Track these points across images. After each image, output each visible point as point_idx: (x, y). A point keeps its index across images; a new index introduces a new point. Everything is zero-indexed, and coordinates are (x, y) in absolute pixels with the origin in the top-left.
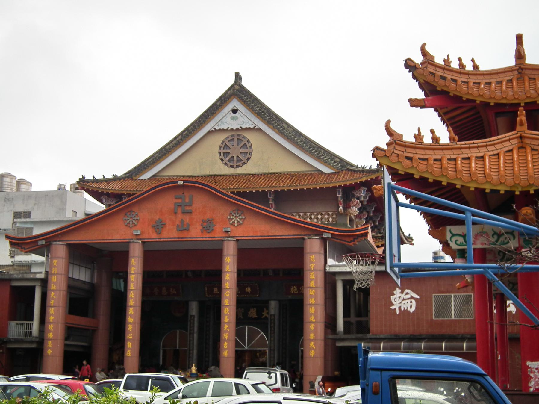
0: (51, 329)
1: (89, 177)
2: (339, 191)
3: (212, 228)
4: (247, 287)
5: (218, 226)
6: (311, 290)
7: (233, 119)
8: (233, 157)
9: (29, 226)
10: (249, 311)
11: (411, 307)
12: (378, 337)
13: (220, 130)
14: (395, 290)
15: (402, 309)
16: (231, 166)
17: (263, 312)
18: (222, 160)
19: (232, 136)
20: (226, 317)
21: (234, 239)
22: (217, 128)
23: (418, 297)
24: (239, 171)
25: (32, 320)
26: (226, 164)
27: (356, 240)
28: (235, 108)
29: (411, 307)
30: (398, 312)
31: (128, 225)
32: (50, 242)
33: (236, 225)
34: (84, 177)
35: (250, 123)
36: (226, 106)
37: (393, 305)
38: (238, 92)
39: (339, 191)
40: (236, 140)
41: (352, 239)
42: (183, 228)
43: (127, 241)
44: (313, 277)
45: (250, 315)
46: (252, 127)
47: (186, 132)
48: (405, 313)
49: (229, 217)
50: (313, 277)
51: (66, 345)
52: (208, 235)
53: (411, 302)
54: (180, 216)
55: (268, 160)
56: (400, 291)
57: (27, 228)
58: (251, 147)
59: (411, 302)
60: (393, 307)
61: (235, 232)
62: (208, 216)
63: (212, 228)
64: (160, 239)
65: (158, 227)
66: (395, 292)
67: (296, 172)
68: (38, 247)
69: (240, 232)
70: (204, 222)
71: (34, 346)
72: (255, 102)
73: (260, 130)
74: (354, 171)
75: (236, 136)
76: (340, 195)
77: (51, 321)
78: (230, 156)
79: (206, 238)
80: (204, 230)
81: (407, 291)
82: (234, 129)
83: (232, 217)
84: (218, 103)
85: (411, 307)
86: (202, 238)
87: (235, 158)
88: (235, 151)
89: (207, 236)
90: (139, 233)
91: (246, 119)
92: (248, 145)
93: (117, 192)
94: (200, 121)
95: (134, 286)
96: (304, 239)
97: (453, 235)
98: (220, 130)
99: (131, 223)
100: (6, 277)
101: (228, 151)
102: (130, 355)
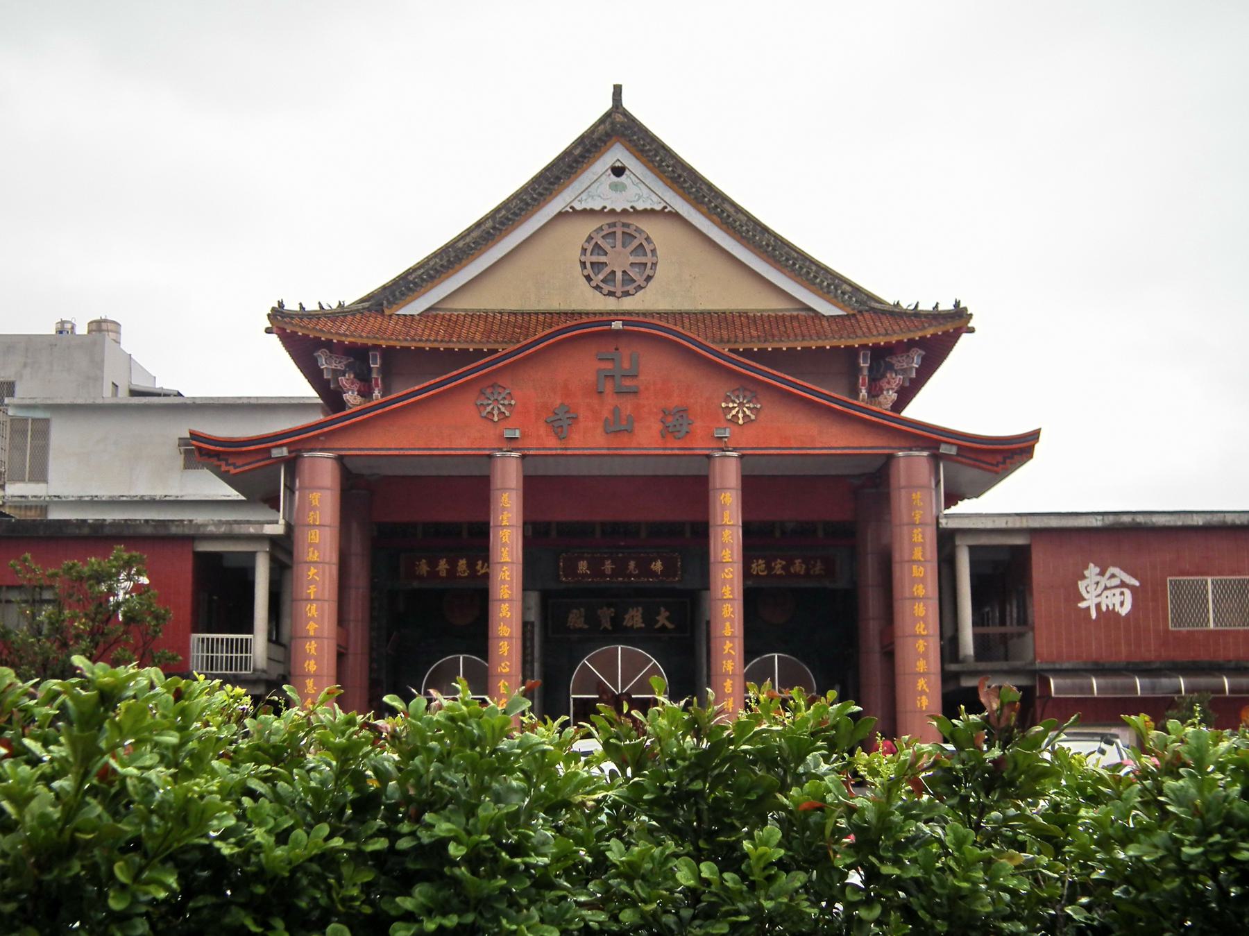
0: (313, 651)
1: (291, 306)
2: (865, 356)
3: (685, 429)
5: (698, 423)
6: (915, 567)
7: (614, 187)
8: (613, 272)
9: (39, 414)
10: (626, 612)
11: (1122, 604)
12: (1058, 666)
13: (585, 211)
14: (1087, 568)
15: (1104, 608)
16: (611, 294)
17: (659, 614)
18: (588, 278)
19: (610, 225)
20: (728, 624)
21: (735, 454)
22: (579, 207)
23: (1137, 583)
24: (628, 304)
25: (250, 630)
26: (597, 288)
28: (618, 164)
30: (1094, 615)
31: (489, 418)
32: (300, 450)
33: (741, 422)
34: (281, 304)
36: (598, 158)
37: (1084, 599)
38: (618, 130)
39: (375, 357)
40: (619, 235)
41: (1000, 458)
42: (619, 428)
43: (487, 452)
44: (918, 538)
45: (627, 622)
46: (658, 208)
47: (503, 212)
48: (1109, 616)
49: (723, 405)
52: (681, 444)
53: (1122, 593)
54: (611, 401)
55: (687, 282)
56: (1097, 570)
57: (34, 420)
58: (653, 251)
59: (1122, 593)
60: (1082, 605)
61: (739, 437)
62: (675, 402)
63: (685, 429)
64: (566, 449)
65: (560, 423)
66: (1086, 573)
67: (759, 311)
68: (267, 462)
69: (750, 439)
70: (665, 413)
72: (662, 152)
73: (675, 215)
74: (884, 312)
76: (864, 364)
78: (607, 270)
79: (672, 449)
80: (667, 432)
81: (1112, 570)
82: (619, 210)
83: (731, 405)
84: (577, 152)
85: (1123, 604)
86: (665, 449)
87: (619, 275)
88: (619, 259)
89: (674, 447)
90: (517, 435)
91: (643, 190)
92: (648, 247)
94: (534, 190)
96: (890, 457)
99: (496, 412)
100: (187, 531)
101: (603, 259)
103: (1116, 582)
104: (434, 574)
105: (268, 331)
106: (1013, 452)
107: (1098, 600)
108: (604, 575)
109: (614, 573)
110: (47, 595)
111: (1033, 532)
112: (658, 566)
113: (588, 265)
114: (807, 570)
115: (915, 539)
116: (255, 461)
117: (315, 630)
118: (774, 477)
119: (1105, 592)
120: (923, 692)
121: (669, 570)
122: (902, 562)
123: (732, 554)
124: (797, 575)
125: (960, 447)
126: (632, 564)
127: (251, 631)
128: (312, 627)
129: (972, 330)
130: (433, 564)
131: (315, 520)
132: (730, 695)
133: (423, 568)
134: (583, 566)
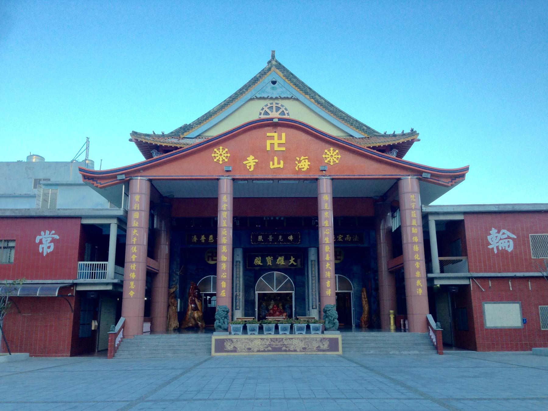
0: (134, 268)
6: (413, 229)
7: (273, 88)
11: (509, 246)
21: (329, 177)
23: (515, 237)
25: (107, 260)
27: (453, 181)
29: (509, 246)
30: (496, 251)
35: (288, 92)
46: (290, 97)
50: (415, 216)
53: (508, 242)
56: (496, 231)
59: (508, 242)
60: (490, 247)
71: (110, 288)
75: (274, 103)
77: (134, 260)
82: (274, 97)
93: (171, 145)
95: (227, 224)
102: (224, 296)
103: (505, 236)
104: (199, 241)
105: (131, 140)
106: (457, 176)
107: (498, 244)
108: (268, 241)
109: (273, 241)
110: (11, 244)
111: (465, 213)
112: (291, 238)
113: (264, 110)
114: (352, 239)
115: (413, 216)
116: (113, 183)
117: (136, 258)
119: (500, 240)
120: (419, 287)
121: (296, 239)
122: (406, 226)
123: (329, 240)
124: (347, 241)
125: (432, 175)
126: (280, 237)
127: (107, 260)
128: (134, 257)
129: (419, 140)
130: (199, 237)
131: (137, 208)
132: (329, 288)
133: (195, 239)
134: (260, 238)
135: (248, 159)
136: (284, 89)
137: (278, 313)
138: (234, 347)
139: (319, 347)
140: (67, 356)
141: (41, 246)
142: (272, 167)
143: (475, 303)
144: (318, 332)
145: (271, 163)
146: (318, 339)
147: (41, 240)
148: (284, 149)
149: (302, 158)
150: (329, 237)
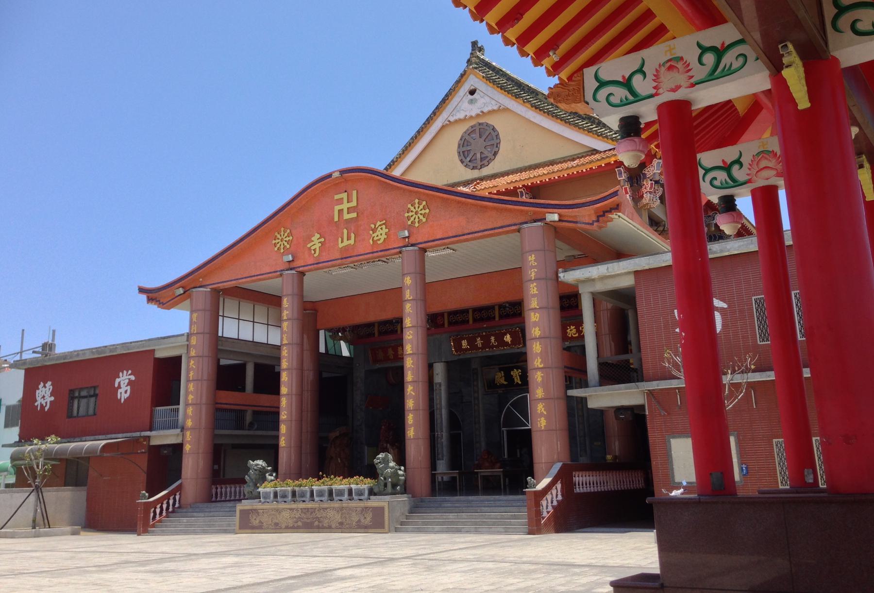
4: (506, 334)
6: (532, 314)
7: (471, 102)
16: (474, 168)
23: (725, 306)
28: (472, 88)
35: (493, 102)
46: (495, 108)
51: (215, 436)
73: (507, 110)
82: (474, 115)
97: (602, 84)
98: (457, 121)
109: (484, 346)
112: (508, 338)
118: (634, 21)
120: (542, 415)
123: (412, 348)
126: (493, 338)
135: (313, 239)
136: (486, 98)
137: (487, 464)
138: (260, 522)
139: (359, 521)
140: (63, 534)
141: (119, 391)
142: (341, 245)
143: (653, 437)
144: (362, 497)
145: (340, 240)
146: (358, 509)
147: (119, 383)
148: (336, 219)
149: (379, 223)
150: (412, 344)
